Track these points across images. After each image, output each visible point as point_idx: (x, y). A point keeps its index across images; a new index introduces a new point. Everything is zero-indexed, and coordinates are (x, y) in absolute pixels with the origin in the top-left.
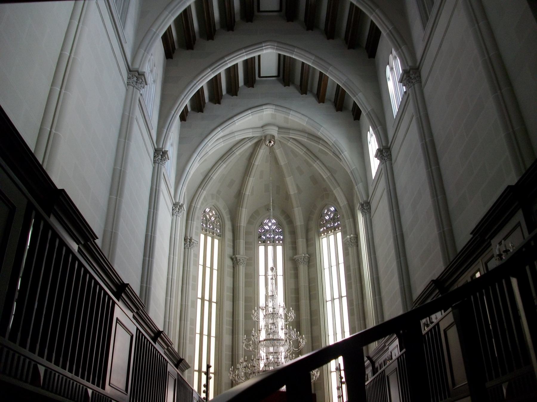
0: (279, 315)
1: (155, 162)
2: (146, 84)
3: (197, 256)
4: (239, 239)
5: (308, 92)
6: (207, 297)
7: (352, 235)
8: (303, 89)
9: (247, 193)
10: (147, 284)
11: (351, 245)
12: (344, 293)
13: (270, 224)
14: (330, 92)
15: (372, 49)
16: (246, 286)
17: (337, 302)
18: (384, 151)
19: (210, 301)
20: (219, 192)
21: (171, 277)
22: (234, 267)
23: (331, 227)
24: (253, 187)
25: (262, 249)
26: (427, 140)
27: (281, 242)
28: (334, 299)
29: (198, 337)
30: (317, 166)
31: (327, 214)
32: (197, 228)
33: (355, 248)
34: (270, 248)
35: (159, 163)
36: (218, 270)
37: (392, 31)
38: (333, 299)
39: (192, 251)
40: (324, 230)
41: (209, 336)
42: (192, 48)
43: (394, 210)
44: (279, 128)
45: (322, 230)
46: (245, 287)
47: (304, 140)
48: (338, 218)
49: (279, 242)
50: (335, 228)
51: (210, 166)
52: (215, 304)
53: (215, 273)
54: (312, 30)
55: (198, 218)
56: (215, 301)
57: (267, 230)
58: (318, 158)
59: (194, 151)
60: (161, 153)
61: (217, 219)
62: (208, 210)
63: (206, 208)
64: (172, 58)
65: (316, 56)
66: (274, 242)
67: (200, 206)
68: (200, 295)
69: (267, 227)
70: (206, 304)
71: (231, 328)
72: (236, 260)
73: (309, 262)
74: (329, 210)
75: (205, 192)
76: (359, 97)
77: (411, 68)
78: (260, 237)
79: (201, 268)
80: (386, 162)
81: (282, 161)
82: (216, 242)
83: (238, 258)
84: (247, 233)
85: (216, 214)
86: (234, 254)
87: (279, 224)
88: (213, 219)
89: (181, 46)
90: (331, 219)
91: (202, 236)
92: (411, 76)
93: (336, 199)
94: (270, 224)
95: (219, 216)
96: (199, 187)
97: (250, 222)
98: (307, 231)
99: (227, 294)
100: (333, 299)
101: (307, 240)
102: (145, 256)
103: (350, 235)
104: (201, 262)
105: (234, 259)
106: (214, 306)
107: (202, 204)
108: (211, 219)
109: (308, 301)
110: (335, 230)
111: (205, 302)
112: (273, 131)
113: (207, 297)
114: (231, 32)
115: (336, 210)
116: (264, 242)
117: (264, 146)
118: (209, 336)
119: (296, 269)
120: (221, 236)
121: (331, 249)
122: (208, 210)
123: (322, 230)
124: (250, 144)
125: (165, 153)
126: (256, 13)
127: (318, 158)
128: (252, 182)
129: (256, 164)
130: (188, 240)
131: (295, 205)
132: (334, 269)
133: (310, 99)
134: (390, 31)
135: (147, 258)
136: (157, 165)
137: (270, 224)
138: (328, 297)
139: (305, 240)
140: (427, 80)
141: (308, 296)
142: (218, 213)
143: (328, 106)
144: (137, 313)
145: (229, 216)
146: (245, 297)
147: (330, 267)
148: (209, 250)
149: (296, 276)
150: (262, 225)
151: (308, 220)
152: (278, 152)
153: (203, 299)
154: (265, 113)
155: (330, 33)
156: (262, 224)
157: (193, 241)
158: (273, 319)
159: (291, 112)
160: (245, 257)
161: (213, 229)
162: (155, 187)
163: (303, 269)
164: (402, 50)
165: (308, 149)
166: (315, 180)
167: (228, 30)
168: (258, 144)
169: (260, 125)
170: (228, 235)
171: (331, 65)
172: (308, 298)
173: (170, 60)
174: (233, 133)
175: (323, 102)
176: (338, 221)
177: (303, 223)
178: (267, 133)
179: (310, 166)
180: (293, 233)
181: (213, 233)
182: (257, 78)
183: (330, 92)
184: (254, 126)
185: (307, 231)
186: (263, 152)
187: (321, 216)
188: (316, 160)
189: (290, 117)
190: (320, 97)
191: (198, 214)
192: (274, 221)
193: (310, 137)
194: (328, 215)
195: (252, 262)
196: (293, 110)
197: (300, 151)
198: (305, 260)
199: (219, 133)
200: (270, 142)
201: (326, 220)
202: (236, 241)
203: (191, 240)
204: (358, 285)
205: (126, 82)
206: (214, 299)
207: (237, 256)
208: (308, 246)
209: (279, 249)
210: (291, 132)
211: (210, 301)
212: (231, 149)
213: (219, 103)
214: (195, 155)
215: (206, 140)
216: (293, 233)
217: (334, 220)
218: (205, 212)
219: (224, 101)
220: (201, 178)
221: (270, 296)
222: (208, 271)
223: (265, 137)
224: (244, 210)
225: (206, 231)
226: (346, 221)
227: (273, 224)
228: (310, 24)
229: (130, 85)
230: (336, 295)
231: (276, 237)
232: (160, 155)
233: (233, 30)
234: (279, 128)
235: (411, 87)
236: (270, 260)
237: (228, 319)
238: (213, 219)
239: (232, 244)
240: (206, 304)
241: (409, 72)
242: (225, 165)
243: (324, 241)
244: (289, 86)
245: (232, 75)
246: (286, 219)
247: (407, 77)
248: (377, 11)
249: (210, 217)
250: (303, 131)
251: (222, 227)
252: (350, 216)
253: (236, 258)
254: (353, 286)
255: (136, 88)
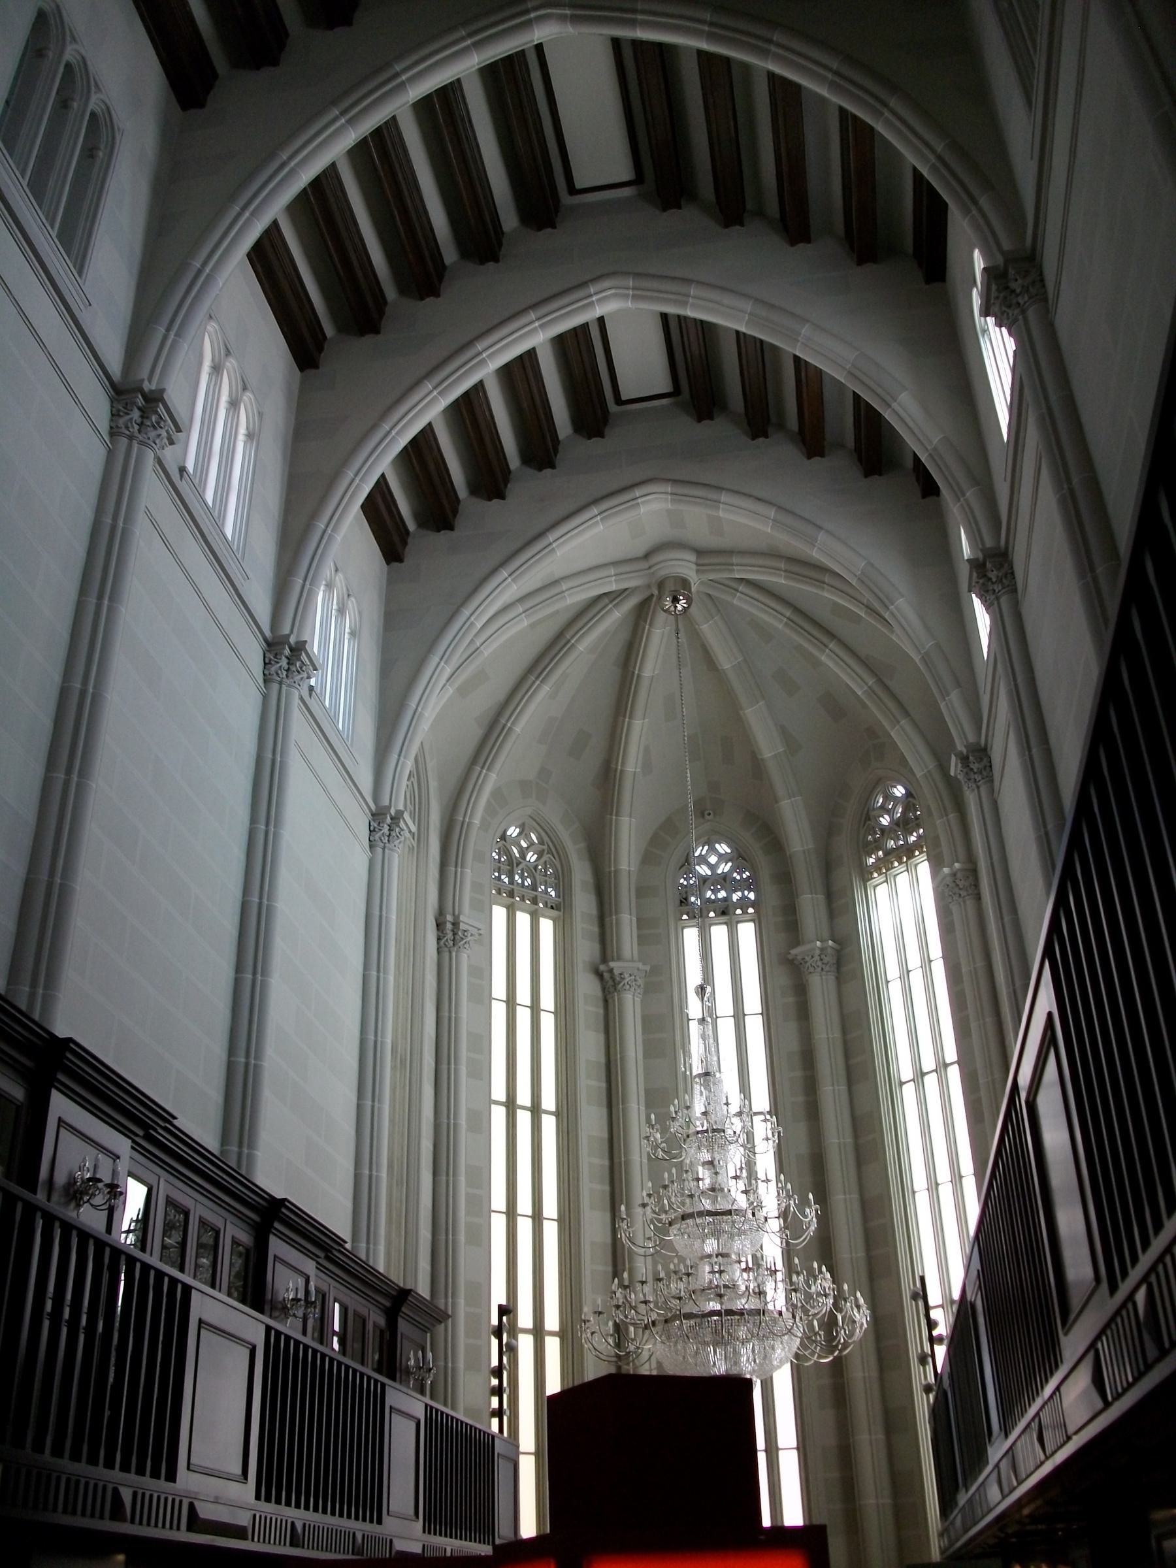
0: (729, 1132)
1: (267, 680)
2: (179, 430)
3: (483, 972)
4: (617, 913)
5: (770, 430)
6: (524, 1097)
7: (957, 865)
8: (759, 422)
9: (630, 768)
10: (247, 1056)
11: (960, 895)
12: (951, 1054)
13: (713, 859)
14: (841, 423)
15: (933, 262)
16: (647, 1055)
17: (931, 1081)
18: (989, 565)
19: (536, 1110)
20: (544, 774)
21: (371, 1037)
22: (606, 1001)
23: (899, 848)
24: (647, 750)
25: (691, 936)
26: (1075, 480)
27: (751, 910)
28: (923, 1074)
29: (498, 1224)
30: (829, 660)
31: (884, 809)
32: (477, 887)
33: (970, 903)
34: (719, 933)
35: (281, 683)
36: (556, 1013)
37: (948, 157)
38: (919, 1075)
39: (465, 959)
40: (878, 859)
41: (537, 1217)
42: (375, 329)
43: (1034, 751)
44: (700, 552)
45: (871, 861)
46: (645, 1057)
47: (778, 580)
48: (917, 818)
49: (745, 912)
50: (908, 852)
51: (501, 696)
52: (553, 1119)
53: (548, 1023)
54: (742, 225)
55: (480, 857)
56: (553, 1108)
57: (704, 880)
58: (832, 635)
59: (430, 650)
60: (287, 651)
61: (546, 857)
62: (513, 831)
63: (507, 827)
64: (315, 366)
65: (780, 508)
66: (725, 911)
67: (483, 819)
68: (499, 1092)
69: (703, 870)
70: (524, 1119)
71: (607, 1188)
72: (613, 978)
73: (839, 963)
74: (888, 797)
75: (493, 776)
76: (914, 417)
77: (1011, 259)
78: (684, 901)
79: (499, 1012)
80: (998, 599)
81: (726, 660)
82: (546, 926)
83: (616, 972)
84: (642, 892)
85: (541, 842)
86: (604, 959)
87: (740, 858)
88: (531, 857)
89: (343, 328)
90: (896, 823)
91: (499, 914)
92: (1013, 285)
93: (903, 761)
94: (714, 859)
95: (551, 848)
96: (474, 761)
97: (648, 859)
98: (828, 867)
99: (590, 1084)
100: (919, 1075)
101: (830, 896)
102: (239, 968)
103: (951, 866)
104: (499, 988)
105: (606, 975)
106: (549, 1125)
107: (490, 810)
108: (523, 856)
109: (843, 1088)
110: (911, 856)
111: (519, 1112)
112: (684, 566)
113: (524, 1097)
114: (548, 472)
115: (909, 794)
116: (700, 918)
117: (661, 617)
118: (537, 1217)
119: (801, 990)
120: (561, 909)
121: (902, 911)
122: (513, 831)
123: (871, 861)
124: (616, 615)
125: (299, 649)
126: (566, 199)
127: (832, 635)
128: (640, 731)
129: (647, 673)
130: (449, 926)
131: (780, 790)
132: (917, 978)
133: (781, 451)
134: (940, 158)
135: (249, 976)
136: (275, 687)
137: (713, 859)
138: (906, 1071)
139: (821, 897)
140: (1058, 283)
141: (842, 1072)
142: (546, 839)
143: (839, 464)
144: (327, 1258)
145: (582, 845)
146: (647, 1091)
147: (905, 973)
148: (521, 954)
149: (803, 1012)
150: (687, 863)
151: (826, 832)
152: (709, 630)
153: (511, 1105)
154: (642, 510)
155: (795, 227)
156: (687, 860)
157: (462, 926)
158: (711, 1149)
159: (724, 497)
160: (640, 965)
161: (534, 887)
162: (269, 755)
163: (821, 987)
164: (980, 210)
165: (797, 610)
166: (835, 707)
167: (483, 261)
168: (643, 613)
169: (641, 552)
170: (584, 902)
171: (805, 321)
172: (843, 1079)
173: (311, 372)
174: (556, 582)
175: (822, 455)
176: (918, 826)
177: (811, 846)
178: (663, 573)
179: (817, 664)
180: (785, 878)
181: (535, 901)
182: (613, 408)
183: (841, 423)
184: (619, 555)
185: (828, 867)
186: (659, 637)
187: (867, 817)
188: (825, 640)
189: (721, 514)
190: (813, 441)
191: (479, 843)
192: (723, 848)
193: (796, 569)
194: (888, 812)
195: (663, 977)
196: (728, 490)
197: (774, 620)
198: (826, 959)
199: (508, 588)
200: (675, 600)
201: (883, 830)
202: (607, 920)
203: (456, 924)
204: (989, 1020)
205: (104, 425)
206: (549, 1101)
207: (612, 964)
208: (832, 914)
209: (747, 932)
210: (735, 560)
211: (536, 1110)
212: (560, 635)
213: (501, 495)
214: (435, 659)
215: (466, 612)
216: (785, 878)
217: (904, 825)
218: (503, 837)
219: (515, 490)
220: (478, 733)
221: (699, 1076)
222: (523, 1017)
223: (661, 585)
224: (625, 820)
225: (511, 894)
226: (938, 822)
227: (722, 858)
228: (731, 210)
229: (120, 434)
230: (928, 1063)
231: (736, 897)
232: (284, 655)
233: (497, 260)
234: (700, 552)
235: (1016, 320)
236: (723, 971)
237: (596, 1161)
238: (531, 857)
239: (596, 929)
240: (524, 1119)
241: (967, 758)
242: (546, 688)
243: (882, 892)
244: (712, 418)
245: (525, 405)
246: (761, 843)
247: (979, 577)
248: (893, 102)
249: (523, 854)
250: (773, 554)
251: (563, 882)
252: (949, 804)
253: (611, 971)
254: (973, 1025)
255: (141, 443)
